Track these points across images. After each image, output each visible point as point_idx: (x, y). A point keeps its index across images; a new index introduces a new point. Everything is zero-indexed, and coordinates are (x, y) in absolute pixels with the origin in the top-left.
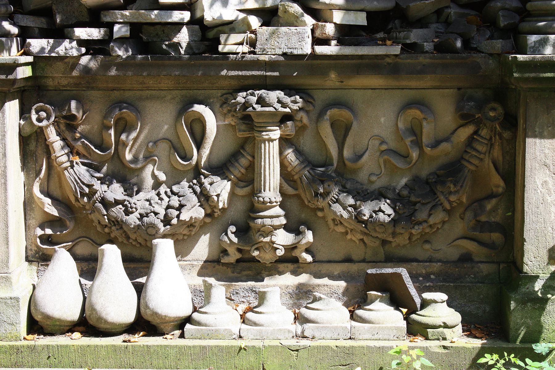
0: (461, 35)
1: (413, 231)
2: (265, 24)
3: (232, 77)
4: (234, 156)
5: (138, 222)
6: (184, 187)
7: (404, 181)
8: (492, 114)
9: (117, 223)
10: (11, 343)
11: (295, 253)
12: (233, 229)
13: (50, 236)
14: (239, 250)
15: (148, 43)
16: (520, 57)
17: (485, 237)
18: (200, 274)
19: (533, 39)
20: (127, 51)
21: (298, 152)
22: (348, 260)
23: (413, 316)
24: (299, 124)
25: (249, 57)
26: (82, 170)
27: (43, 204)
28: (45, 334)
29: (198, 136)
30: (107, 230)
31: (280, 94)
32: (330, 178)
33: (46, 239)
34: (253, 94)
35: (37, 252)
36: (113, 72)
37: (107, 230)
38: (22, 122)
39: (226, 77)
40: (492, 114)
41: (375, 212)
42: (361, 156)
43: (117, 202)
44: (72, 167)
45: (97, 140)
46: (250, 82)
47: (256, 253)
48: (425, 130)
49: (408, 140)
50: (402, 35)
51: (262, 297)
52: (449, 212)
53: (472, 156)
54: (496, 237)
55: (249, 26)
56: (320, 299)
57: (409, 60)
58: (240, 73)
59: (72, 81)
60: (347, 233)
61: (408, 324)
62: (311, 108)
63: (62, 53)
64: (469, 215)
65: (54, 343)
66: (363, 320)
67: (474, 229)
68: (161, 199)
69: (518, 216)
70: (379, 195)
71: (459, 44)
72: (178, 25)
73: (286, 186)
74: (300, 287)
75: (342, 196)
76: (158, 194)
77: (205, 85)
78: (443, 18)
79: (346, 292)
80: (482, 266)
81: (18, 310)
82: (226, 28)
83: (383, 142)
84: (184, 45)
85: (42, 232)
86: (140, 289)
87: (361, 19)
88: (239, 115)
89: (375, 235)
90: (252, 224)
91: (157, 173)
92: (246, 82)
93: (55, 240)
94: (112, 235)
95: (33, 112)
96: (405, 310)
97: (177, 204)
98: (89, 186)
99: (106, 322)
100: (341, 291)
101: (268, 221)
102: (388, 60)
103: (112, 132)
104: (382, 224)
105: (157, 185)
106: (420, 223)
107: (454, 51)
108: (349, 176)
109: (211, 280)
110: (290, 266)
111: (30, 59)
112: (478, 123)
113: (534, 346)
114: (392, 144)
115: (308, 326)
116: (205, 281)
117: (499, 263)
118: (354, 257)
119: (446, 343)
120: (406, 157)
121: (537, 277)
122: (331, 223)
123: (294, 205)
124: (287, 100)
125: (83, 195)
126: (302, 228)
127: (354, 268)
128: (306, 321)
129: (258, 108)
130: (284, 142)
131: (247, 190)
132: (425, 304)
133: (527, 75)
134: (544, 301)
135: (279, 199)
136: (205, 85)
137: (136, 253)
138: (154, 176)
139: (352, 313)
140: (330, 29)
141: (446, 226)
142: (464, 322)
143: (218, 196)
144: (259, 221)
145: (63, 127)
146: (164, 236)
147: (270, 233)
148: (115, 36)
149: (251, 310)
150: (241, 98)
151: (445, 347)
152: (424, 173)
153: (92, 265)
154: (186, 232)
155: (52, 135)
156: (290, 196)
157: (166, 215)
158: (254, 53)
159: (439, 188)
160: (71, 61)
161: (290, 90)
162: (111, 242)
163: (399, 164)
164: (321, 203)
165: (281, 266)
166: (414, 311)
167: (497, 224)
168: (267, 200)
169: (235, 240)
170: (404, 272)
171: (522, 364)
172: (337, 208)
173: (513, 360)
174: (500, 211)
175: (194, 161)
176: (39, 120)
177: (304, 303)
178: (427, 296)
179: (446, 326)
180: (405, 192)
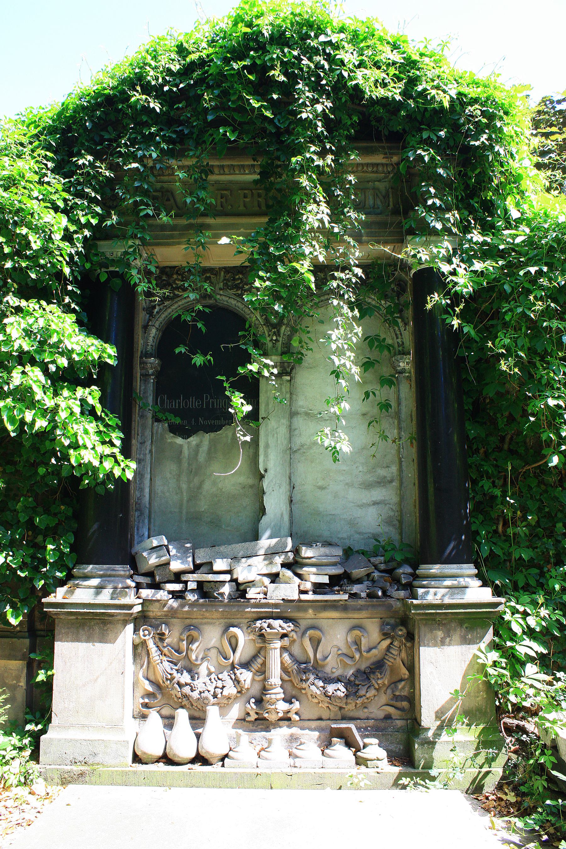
0: (381, 588)
1: (358, 702)
2: (273, 582)
3: (254, 612)
4: (254, 657)
5: (199, 696)
6: (225, 676)
7: (351, 672)
8: (400, 633)
9: (186, 696)
10: (123, 769)
11: (289, 715)
12: (253, 700)
13: (147, 703)
14: (257, 713)
15: (206, 592)
16: (415, 602)
17: (399, 704)
18: (234, 727)
19: (421, 591)
20: (194, 596)
21: (291, 655)
22: (320, 719)
23: (359, 753)
24: (292, 639)
25: (263, 601)
26: (167, 665)
27: (144, 684)
28: (142, 763)
29: (234, 646)
30: (180, 700)
31: (280, 622)
32: (309, 670)
33: (146, 706)
34: (265, 622)
35: (139, 713)
36: (186, 609)
37: (180, 700)
38: (134, 636)
39: (250, 612)
40: (400, 633)
41: (335, 690)
42: (327, 658)
43: (187, 684)
44: (162, 663)
45: (176, 648)
46: (264, 615)
47: (266, 715)
48: (363, 643)
49: (354, 648)
50: (349, 588)
51: (270, 742)
52: (378, 690)
53: (390, 657)
54: (405, 704)
55: (263, 583)
56: (304, 743)
57: (352, 602)
58: (258, 610)
59: (163, 613)
60: (319, 703)
61: (356, 758)
62: (298, 629)
63: (159, 598)
64: (389, 691)
65: (148, 770)
66: (329, 757)
67: (392, 700)
68: (212, 682)
69: (417, 692)
70: (338, 680)
71: (380, 593)
72: (223, 582)
73: (284, 675)
74: (292, 735)
75: (316, 681)
76: (210, 680)
77: (238, 616)
78: (371, 578)
79: (319, 738)
80: (397, 722)
81: (128, 748)
82: (250, 584)
83: (339, 649)
84: (227, 593)
85: (143, 701)
86: (198, 736)
87: (326, 580)
88: (257, 634)
89: (335, 704)
90: (264, 698)
91: (210, 667)
92: (262, 615)
93: (150, 705)
94: (183, 704)
95: (141, 630)
96: (354, 750)
97: (221, 686)
98: (170, 674)
99: (178, 757)
100: (316, 737)
101: (273, 696)
102: (341, 602)
103: (185, 643)
104: (340, 698)
105: (210, 674)
106: (361, 697)
107: (377, 597)
108: (320, 669)
109: (240, 731)
110: (286, 723)
111: (141, 601)
112: (393, 638)
113: (430, 771)
114: (344, 651)
115: (297, 760)
116: (236, 732)
117: (407, 720)
118: (324, 717)
119: (379, 770)
120: (352, 658)
121: (429, 729)
122: (310, 697)
123: (288, 686)
124: (285, 625)
125: (167, 679)
126: (293, 700)
127: (323, 724)
128: (296, 757)
129: (268, 630)
130: (284, 649)
131: (262, 677)
132: (365, 746)
133: (418, 612)
134: (434, 743)
135: (280, 683)
136: (238, 616)
137: (197, 714)
138: (208, 669)
139: (323, 751)
140: (308, 586)
141: (376, 698)
142: (389, 756)
143: (245, 681)
144: (268, 696)
145: (157, 640)
146: (213, 705)
147: (274, 703)
148: (189, 589)
149: (263, 749)
150: (258, 624)
151: (378, 773)
152: (363, 667)
153: (171, 721)
154: (226, 702)
155: (151, 645)
156: (286, 681)
157: (214, 692)
158: (266, 598)
159: (372, 676)
160: (164, 602)
161: (286, 619)
162: (182, 707)
163: (349, 661)
164: (304, 685)
165: (281, 723)
166: (359, 750)
167: (405, 696)
168: (273, 683)
169: (254, 707)
170: (352, 726)
171: (424, 783)
172: (313, 688)
173: (419, 781)
174: (407, 689)
175: (231, 661)
176: (144, 636)
177: (295, 745)
178: (367, 740)
179: (378, 760)
180: (352, 679)
